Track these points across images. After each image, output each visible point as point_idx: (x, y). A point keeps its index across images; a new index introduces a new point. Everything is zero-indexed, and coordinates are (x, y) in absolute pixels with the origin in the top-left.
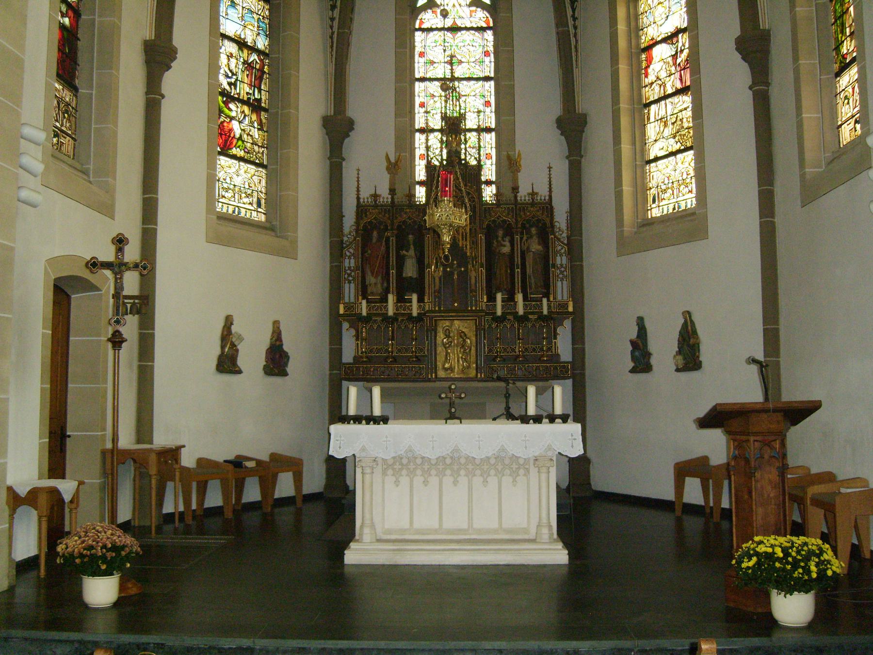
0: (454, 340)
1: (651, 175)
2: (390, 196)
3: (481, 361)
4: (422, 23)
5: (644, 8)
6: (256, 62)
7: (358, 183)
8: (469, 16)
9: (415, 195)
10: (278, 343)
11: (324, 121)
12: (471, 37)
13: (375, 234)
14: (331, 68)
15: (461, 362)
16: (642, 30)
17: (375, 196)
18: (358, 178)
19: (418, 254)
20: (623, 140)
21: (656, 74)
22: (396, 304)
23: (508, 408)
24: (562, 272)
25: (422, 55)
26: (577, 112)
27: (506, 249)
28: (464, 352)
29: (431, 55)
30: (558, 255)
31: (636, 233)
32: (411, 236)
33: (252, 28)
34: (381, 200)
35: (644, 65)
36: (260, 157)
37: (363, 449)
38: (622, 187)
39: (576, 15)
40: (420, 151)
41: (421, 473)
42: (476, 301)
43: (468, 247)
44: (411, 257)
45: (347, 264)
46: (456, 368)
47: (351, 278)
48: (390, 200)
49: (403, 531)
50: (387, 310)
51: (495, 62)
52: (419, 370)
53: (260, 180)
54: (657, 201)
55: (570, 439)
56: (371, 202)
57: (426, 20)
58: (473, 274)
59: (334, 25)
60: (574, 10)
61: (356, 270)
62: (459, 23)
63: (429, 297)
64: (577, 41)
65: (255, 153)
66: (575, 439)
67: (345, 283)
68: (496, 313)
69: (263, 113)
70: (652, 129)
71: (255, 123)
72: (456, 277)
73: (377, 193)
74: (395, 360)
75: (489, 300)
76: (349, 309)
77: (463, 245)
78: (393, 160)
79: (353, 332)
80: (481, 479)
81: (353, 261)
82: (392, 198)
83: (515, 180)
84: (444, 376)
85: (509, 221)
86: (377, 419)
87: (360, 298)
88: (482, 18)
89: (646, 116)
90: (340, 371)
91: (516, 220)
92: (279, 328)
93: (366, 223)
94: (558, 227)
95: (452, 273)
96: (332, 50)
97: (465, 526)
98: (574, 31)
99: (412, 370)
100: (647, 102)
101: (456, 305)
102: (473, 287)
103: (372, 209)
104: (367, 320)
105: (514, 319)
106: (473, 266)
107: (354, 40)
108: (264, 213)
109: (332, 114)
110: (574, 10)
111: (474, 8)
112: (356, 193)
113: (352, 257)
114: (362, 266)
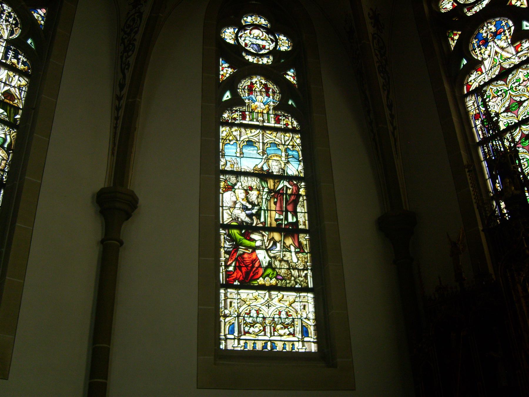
6: (287, 188)
65: (293, 278)
108: (314, 342)
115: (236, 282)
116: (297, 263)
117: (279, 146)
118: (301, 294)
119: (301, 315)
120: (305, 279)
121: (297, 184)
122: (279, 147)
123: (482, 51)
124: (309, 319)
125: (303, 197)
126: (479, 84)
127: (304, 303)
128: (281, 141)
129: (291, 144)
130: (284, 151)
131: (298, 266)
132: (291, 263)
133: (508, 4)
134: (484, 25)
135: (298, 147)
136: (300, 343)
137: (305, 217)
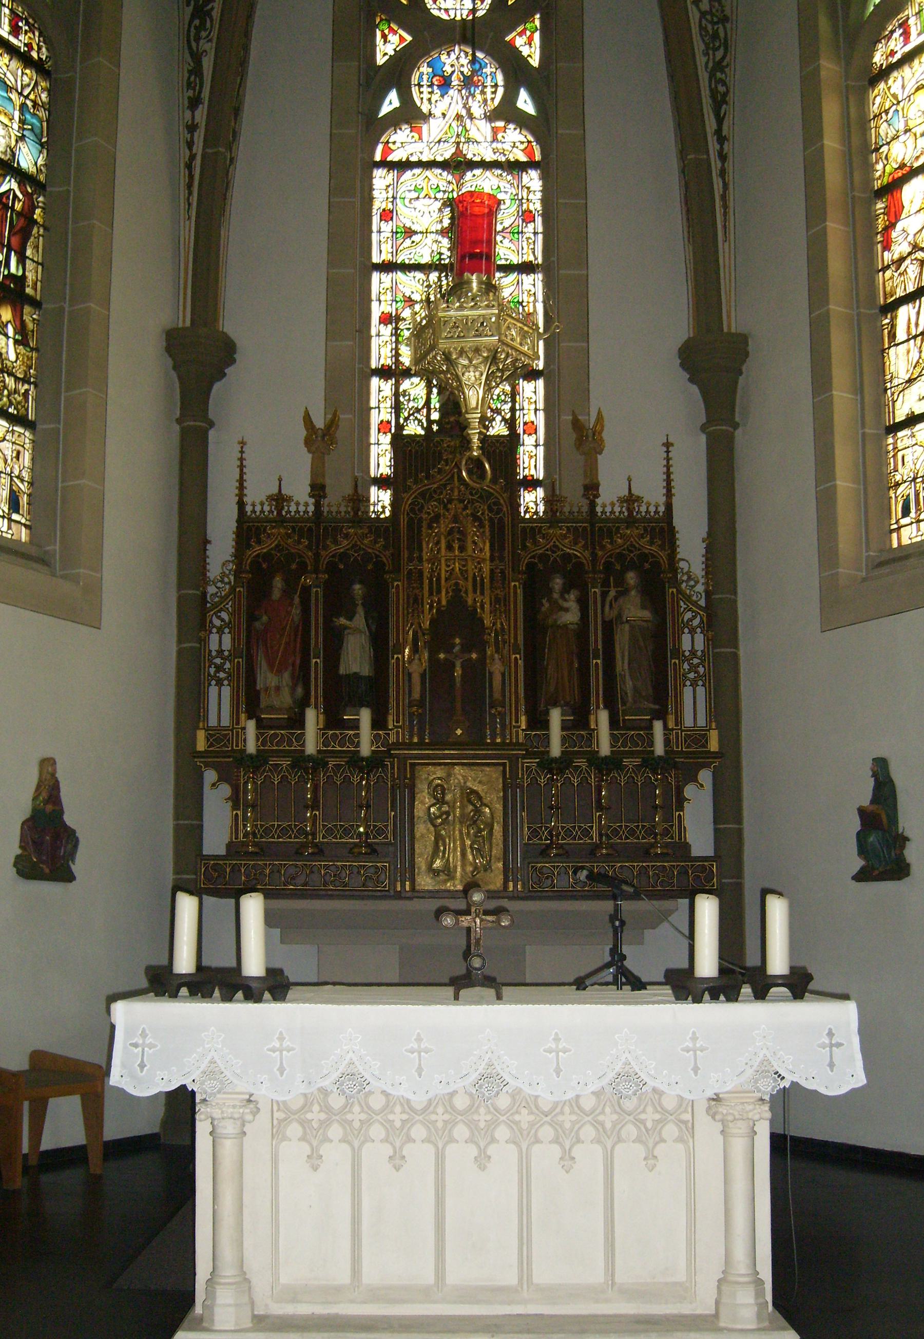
0: (454, 807)
1: (900, 454)
2: (312, 500)
4: (387, 151)
5: (882, 104)
6: (15, 196)
7: (241, 470)
8: (489, 139)
9: (368, 500)
10: (49, 808)
11: (167, 340)
13: (278, 582)
14: (188, 231)
15: (471, 857)
16: (877, 150)
17: (279, 499)
18: (241, 459)
19: (373, 627)
20: (835, 381)
21: (910, 238)
22: (322, 731)
23: (617, 957)
24: (693, 668)
25: (387, 215)
26: (725, 330)
27: (571, 617)
28: (476, 836)
29: (406, 216)
30: (686, 630)
31: (864, 580)
32: (357, 587)
33: (6, 121)
35: (881, 223)
36: (19, 403)
37: (212, 1073)
38: (834, 479)
39: (724, 133)
40: (381, 412)
41: (383, 1134)
42: (503, 726)
43: (487, 606)
44: (357, 631)
45: (214, 646)
46: (459, 869)
47: (222, 675)
48: (311, 508)
49: (333, 1292)
50: (303, 745)
51: (546, 234)
53: (18, 453)
54: (913, 510)
55: (823, 1046)
56: (271, 512)
58: (497, 668)
59: (196, 140)
60: (720, 121)
61: (235, 658)
63: (398, 716)
64: (725, 186)
65: (6, 392)
66: (839, 1045)
67: (210, 685)
69: (27, 309)
70: (900, 356)
71: (10, 326)
72: (458, 672)
73: (283, 492)
74: (320, 851)
75: (531, 725)
76: (218, 740)
78: (319, 422)
79: (226, 790)
80: (556, 1150)
81: (227, 639)
82: (317, 505)
83: (591, 468)
84: (430, 888)
86: (254, 985)
87: (243, 716)
88: (518, 144)
89: (886, 331)
90: (196, 874)
91: (594, 555)
92: (53, 775)
93: (258, 555)
96: (190, 193)
97: (511, 1279)
98: (719, 164)
99: (359, 872)
100: (890, 300)
101: (459, 732)
102: (497, 695)
103: (273, 528)
104: (258, 762)
105: (590, 766)
107: (240, 174)
108: (25, 525)
109: (188, 323)
110: (720, 121)
111: (501, 124)
112: (237, 491)
114: (248, 650)
115: (543, 605)
116: (15, 364)
117: (11, 92)
118: (15, 428)
119: (11, 469)
120: (23, 401)
121: (32, 194)
122: (10, 95)
123: (435, 97)
124: (22, 481)
125: (39, 228)
126: (408, 158)
127: (18, 448)
128: (16, 81)
129: (32, 97)
130: (18, 108)
131: (16, 371)
132: (6, 359)
133: (508, 39)
134: (454, 50)
135: (42, 109)
136: (6, 520)
137: (37, 272)
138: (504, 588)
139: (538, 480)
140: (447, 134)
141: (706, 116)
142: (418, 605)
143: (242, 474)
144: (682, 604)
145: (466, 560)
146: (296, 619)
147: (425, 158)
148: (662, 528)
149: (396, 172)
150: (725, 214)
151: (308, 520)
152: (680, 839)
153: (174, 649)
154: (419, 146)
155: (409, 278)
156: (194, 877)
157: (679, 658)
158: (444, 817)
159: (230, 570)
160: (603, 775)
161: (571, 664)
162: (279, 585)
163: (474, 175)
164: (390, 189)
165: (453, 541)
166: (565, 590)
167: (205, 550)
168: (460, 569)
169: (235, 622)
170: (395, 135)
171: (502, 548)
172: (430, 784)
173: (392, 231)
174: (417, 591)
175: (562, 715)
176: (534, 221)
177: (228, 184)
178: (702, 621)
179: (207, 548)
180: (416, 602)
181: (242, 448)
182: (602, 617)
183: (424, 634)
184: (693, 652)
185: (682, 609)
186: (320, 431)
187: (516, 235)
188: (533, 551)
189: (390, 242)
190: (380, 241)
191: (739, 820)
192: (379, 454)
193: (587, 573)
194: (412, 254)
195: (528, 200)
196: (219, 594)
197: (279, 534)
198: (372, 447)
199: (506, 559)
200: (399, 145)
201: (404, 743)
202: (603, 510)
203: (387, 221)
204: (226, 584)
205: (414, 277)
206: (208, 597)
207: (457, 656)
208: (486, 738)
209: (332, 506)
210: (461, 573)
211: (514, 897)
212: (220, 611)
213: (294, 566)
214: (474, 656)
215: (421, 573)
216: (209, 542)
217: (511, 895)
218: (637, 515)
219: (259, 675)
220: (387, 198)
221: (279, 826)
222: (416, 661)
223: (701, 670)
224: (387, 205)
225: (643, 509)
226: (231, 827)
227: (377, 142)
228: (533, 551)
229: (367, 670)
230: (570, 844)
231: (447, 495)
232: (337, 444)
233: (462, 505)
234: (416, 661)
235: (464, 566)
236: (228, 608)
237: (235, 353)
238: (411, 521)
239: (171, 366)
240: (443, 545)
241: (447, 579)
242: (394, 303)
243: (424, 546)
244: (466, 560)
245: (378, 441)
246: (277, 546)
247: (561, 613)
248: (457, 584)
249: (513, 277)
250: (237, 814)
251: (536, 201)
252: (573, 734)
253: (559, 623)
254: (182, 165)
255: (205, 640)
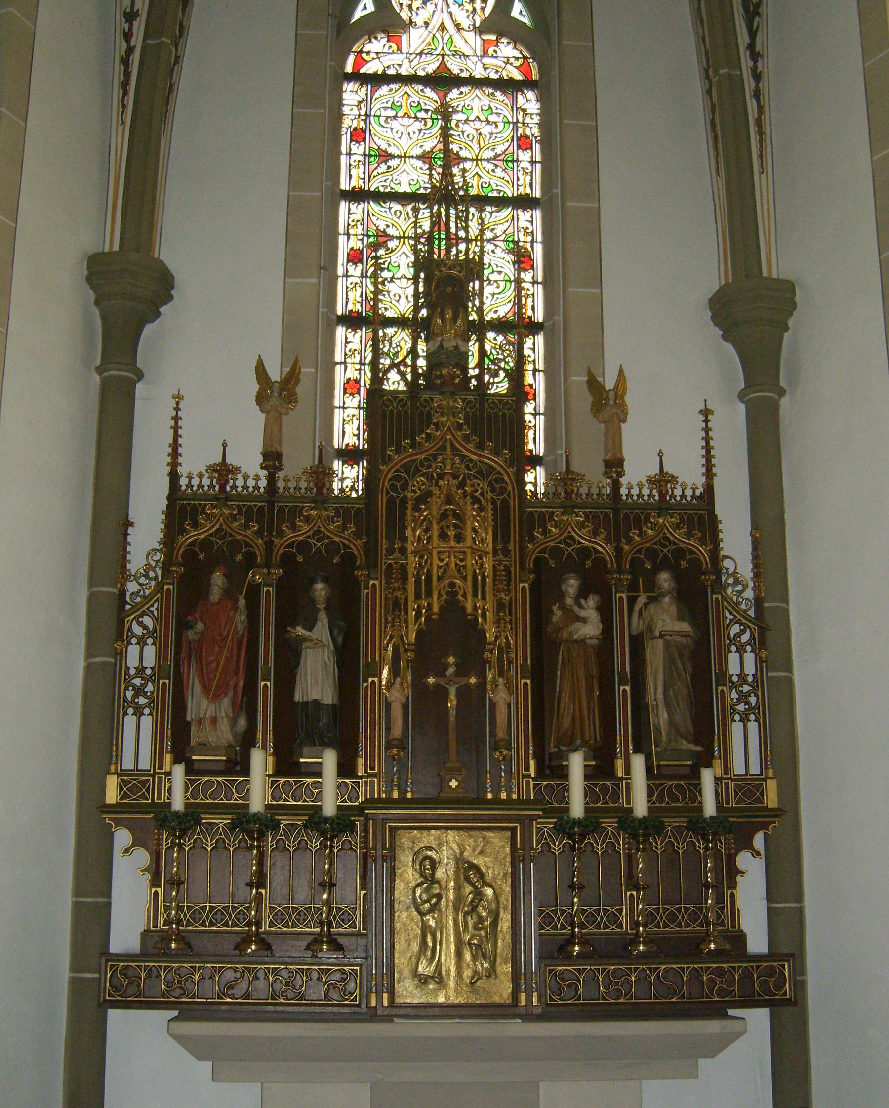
3: (528, 953)
4: (360, 61)
8: (479, 53)
12: (486, 101)
13: (218, 579)
14: (120, 139)
18: (176, 418)
19: (340, 640)
24: (743, 698)
25: (358, 135)
26: (765, 274)
30: (733, 648)
32: (319, 586)
34: (240, 483)
39: (758, 48)
44: (319, 644)
45: (132, 662)
47: (142, 701)
48: (263, 483)
50: (247, 797)
52: (343, 980)
56: (211, 486)
57: (373, 55)
58: (500, 696)
60: (753, 34)
62: (455, 67)
64: (761, 109)
67: (125, 714)
68: (567, 810)
72: (452, 702)
73: (229, 461)
77: (475, 608)
78: (275, 374)
79: (142, 857)
81: (150, 652)
82: (271, 479)
83: (614, 439)
85: (597, 551)
87: (168, 758)
91: (619, 550)
94: (731, 571)
95: (441, 693)
96: (125, 93)
98: (753, 84)
99: (319, 979)
101: (454, 784)
102: (501, 734)
106: (501, 674)
109: (116, 248)
110: (753, 34)
112: (169, 459)
113: (150, 641)
114: (177, 666)
138: (509, 590)
139: (538, 456)
140: (430, 45)
141: (738, 28)
142: (400, 611)
143: (176, 437)
144: (727, 614)
145: (464, 552)
146: (241, 627)
147: (404, 71)
148: (701, 517)
149: (369, 87)
150: (761, 141)
151: (259, 498)
152: (733, 926)
153: (81, 664)
154: (397, 58)
155: (383, 209)
156: (97, 975)
157: (725, 685)
158: (434, 901)
159: (157, 562)
160: (638, 843)
161: (590, 691)
162: (220, 582)
163: (461, 93)
164: (362, 105)
165: (448, 527)
166: (583, 594)
167: (126, 534)
168: (456, 565)
169: (160, 630)
170: (370, 45)
171: (506, 539)
172: (416, 854)
173: (364, 154)
174: (398, 594)
175: (585, 759)
176: (531, 148)
177: (171, 86)
178: (752, 636)
179: (129, 532)
180: (397, 606)
181: (178, 403)
182: (629, 632)
183: (406, 651)
184: (742, 677)
185: (728, 621)
186: (276, 385)
187: (510, 164)
188: (542, 544)
189: (362, 167)
190: (350, 165)
191: (799, 898)
192: (344, 420)
193: (609, 572)
194: (388, 182)
195: (524, 123)
196: (142, 593)
197: (221, 516)
198: (336, 411)
199: (512, 553)
200: (373, 55)
201: (380, 800)
202: (629, 492)
203: (358, 142)
204: (151, 579)
205: (390, 208)
206: (128, 594)
207: (451, 681)
208: (486, 792)
209: (289, 480)
210: (459, 571)
211: (528, 1016)
212: (142, 616)
213: (239, 558)
214: (473, 680)
215: (404, 569)
216: (132, 524)
217: (523, 1012)
218: (670, 499)
219: (190, 697)
220: (359, 115)
221: (212, 908)
222: (397, 686)
223: (753, 700)
224: (359, 124)
225: (678, 492)
226: (149, 910)
227: (349, 52)
228: (542, 544)
229: (331, 697)
230: (594, 934)
231: (437, 468)
232: (297, 402)
233: (456, 482)
234: (397, 686)
235: (461, 560)
236: (152, 612)
237: (173, 288)
238: (391, 501)
239: (93, 300)
240: (435, 533)
241: (439, 579)
242: (365, 238)
243: (408, 533)
244: (464, 552)
245: (344, 403)
246: (220, 530)
247: (578, 625)
248: (452, 585)
249: (506, 212)
250: (156, 892)
251: (533, 125)
252: (596, 785)
253: (575, 637)
254: (117, 61)
255: (121, 654)
